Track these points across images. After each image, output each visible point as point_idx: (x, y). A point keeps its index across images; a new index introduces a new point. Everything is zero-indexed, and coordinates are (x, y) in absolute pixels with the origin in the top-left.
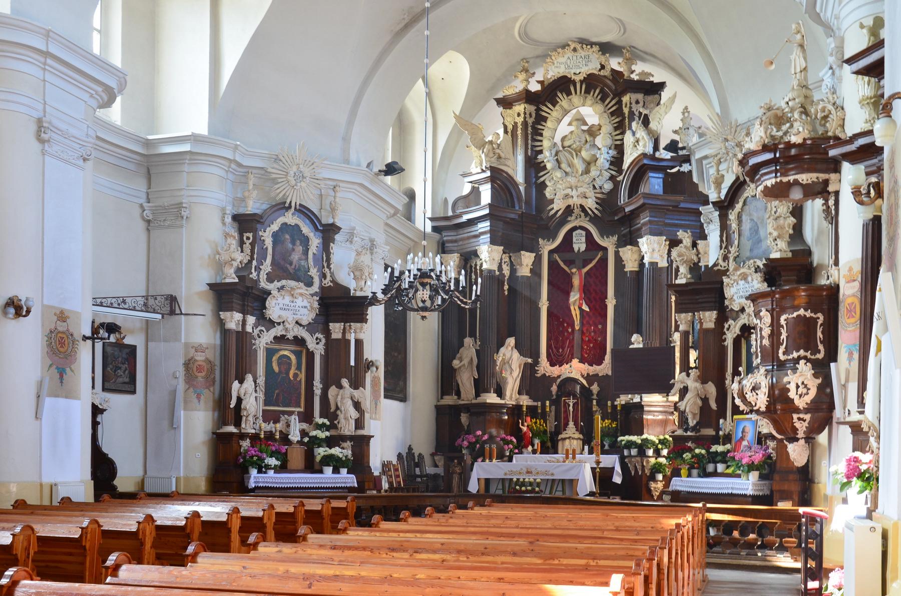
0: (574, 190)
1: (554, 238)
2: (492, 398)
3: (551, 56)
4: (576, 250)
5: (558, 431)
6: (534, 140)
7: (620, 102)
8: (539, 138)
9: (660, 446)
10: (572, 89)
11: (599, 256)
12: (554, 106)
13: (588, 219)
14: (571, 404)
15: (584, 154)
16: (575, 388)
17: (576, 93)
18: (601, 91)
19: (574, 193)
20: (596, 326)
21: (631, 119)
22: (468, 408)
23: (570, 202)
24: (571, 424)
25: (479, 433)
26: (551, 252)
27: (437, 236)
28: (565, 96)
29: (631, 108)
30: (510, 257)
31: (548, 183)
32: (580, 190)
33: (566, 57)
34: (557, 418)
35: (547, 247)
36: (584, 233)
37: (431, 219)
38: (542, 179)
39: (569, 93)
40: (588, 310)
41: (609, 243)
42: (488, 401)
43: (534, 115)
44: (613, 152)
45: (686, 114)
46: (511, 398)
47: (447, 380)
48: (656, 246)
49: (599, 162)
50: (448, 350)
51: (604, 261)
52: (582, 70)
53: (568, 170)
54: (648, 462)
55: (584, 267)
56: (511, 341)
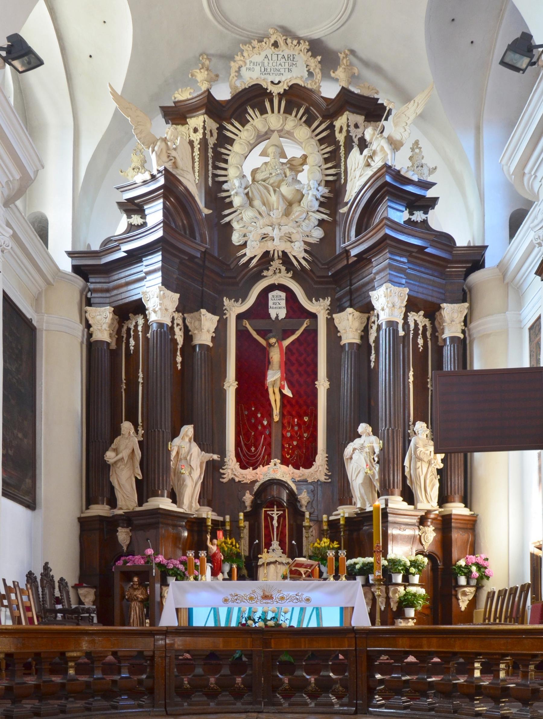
0: (276, 231)
1: (244, 297)
2: (164, 503)
3: (242, 51)
4: (273, 316)
5: (255, 552)
6: (215, 167)
7: (331, 127)
8: (223, 165)
9: (413, 570)
10: (267, 105)
11: (305, 325)
12: (243, 126)
13: (290, 275)
14: (276, 518)
15: (285, 190)
16: (279, 493)
17: (273, 112)
18: (307, 111)
19: (276, 233)
20: (300, 418)
21: (349, 148)
22: (128, 519)
23: (269, 246)
24: (275, 544)
25: (150, 551)
26: (240, 317)
27: (79, 281)
28: (258, 113)
29: (348, 132)
30: (184, 320)
31: (235, 225)
32: (285, 229)
33: (263, 54)
34: (254, 534)
35: (234, 309)
36: (283, 295)
37: (70, 254)
38: (227, 219)
39: (263, 111)
40: (290, 395)
41: (319, 308)
42: (161, 506)
43: (215, 135)
44: (324, 190)
45: (417, 151)
46: (190, 507)
47: (96, 480)
48: (396, 299)
49: (304, 202)
50: (98, 436)
51: (311, 334)
52: (283, 79)
53: (263, 209)
54: (396, 591)
55: (284, 338)
56: (188, 430)
